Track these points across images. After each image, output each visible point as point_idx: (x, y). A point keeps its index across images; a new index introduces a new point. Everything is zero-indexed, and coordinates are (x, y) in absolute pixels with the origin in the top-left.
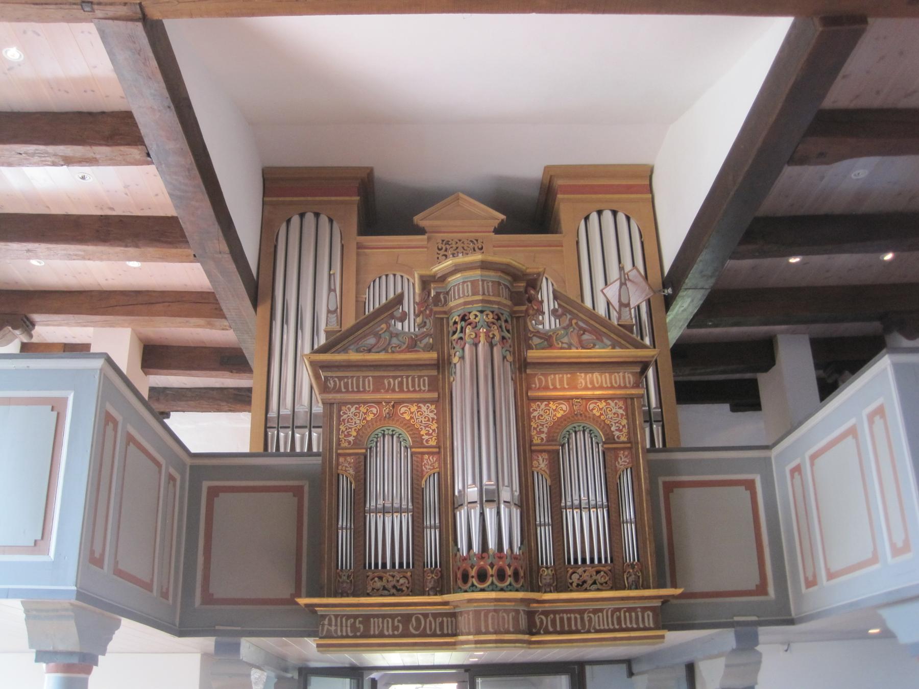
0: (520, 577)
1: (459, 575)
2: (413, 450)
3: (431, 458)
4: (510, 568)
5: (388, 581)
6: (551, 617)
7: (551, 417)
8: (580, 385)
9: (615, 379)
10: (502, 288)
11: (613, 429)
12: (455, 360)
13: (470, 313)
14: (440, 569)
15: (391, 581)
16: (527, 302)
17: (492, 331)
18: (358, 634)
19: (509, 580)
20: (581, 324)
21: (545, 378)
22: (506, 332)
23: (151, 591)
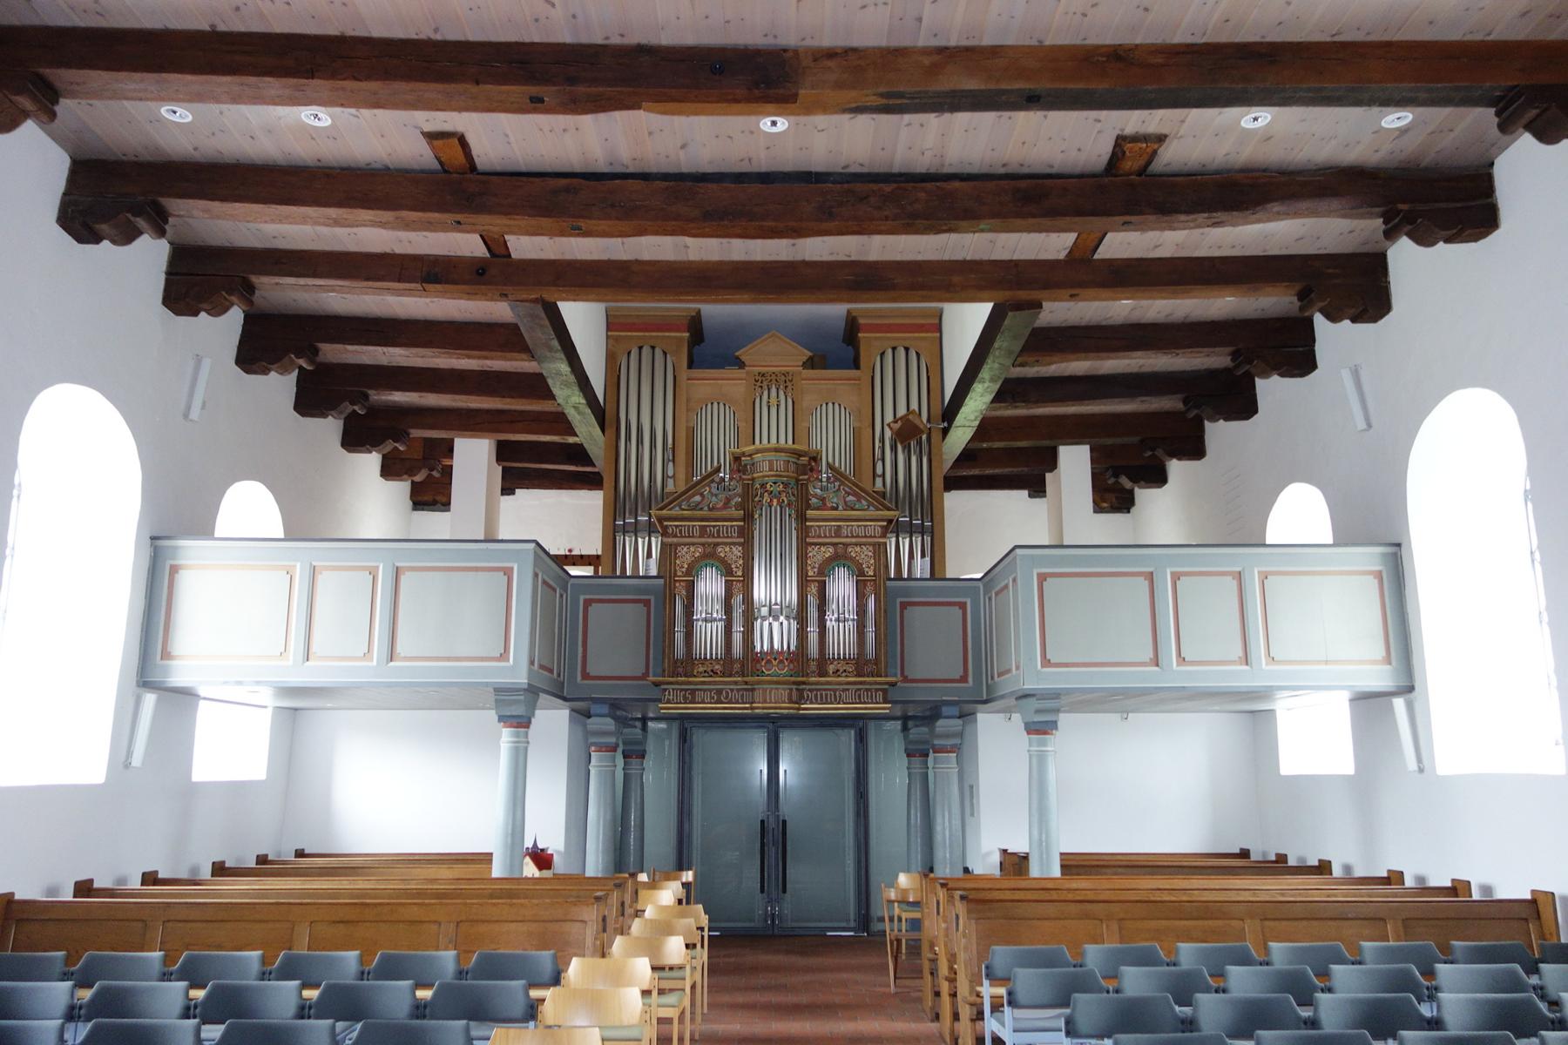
12: (756, 516)
20: (847, 489)
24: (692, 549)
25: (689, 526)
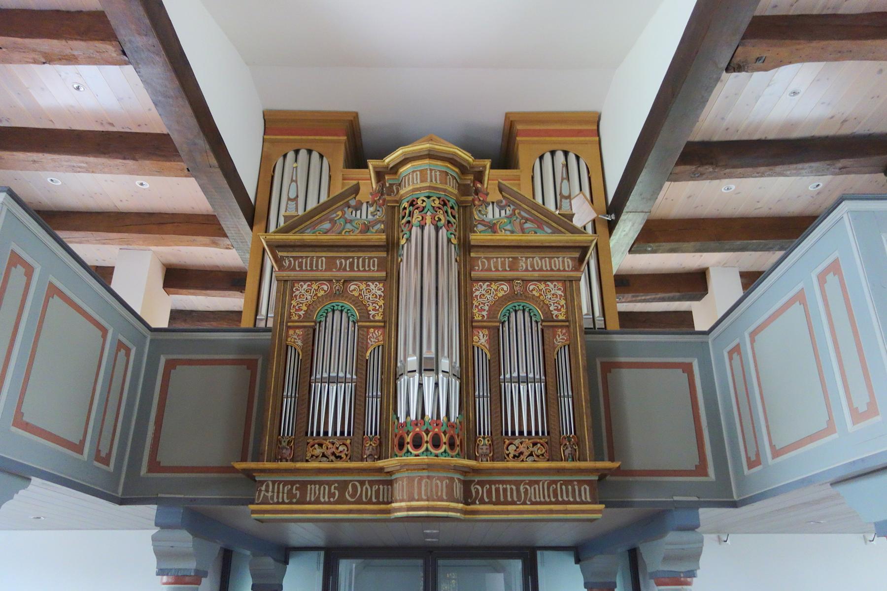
0: (456, 446)
1: (396, 441)
2: (360, 324)
3: (376, 332)
4: (445, 435)
5: (327, 448)
6: (487, 488)
7: (492, 297)
8: (521, 268)
9: (555, 264)
10: (450, 178)
11: (551, 308)
12: (403, 242)
13: (418, 199)
14: (379, 437)
15: (330, 448)
16: (473, 194)
17: (437, 214)
18: (294, 500)
19: (444, 447)
20: (523, 214)
21: (488, 261)
22: (453, 218)
23: (81, 452)
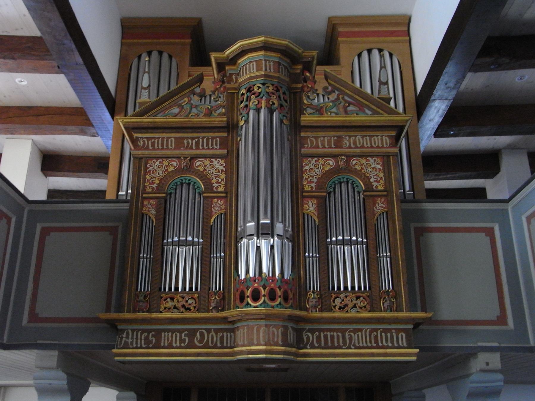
12: (242, 123)
20: (347, 98)
24: (166, 163)
25: (163, 138)
